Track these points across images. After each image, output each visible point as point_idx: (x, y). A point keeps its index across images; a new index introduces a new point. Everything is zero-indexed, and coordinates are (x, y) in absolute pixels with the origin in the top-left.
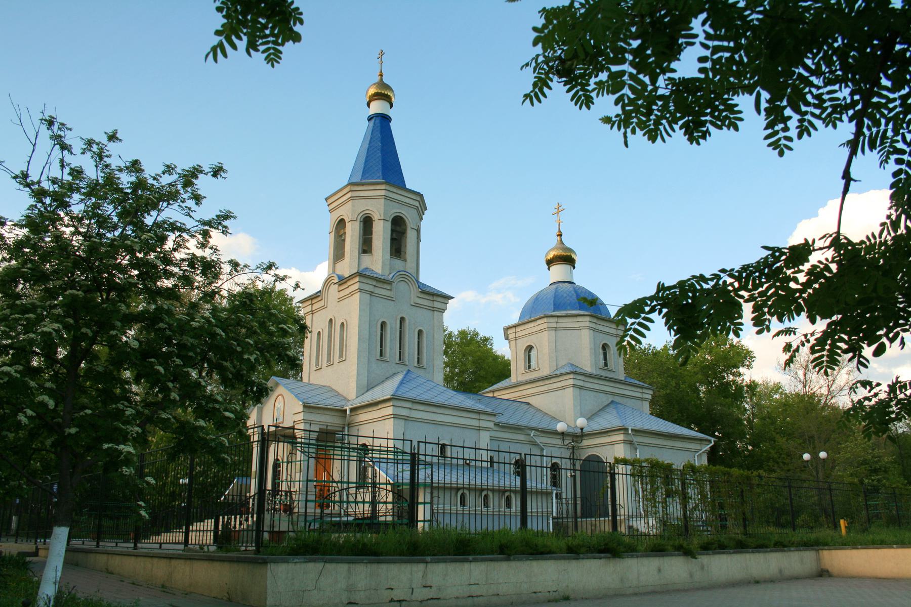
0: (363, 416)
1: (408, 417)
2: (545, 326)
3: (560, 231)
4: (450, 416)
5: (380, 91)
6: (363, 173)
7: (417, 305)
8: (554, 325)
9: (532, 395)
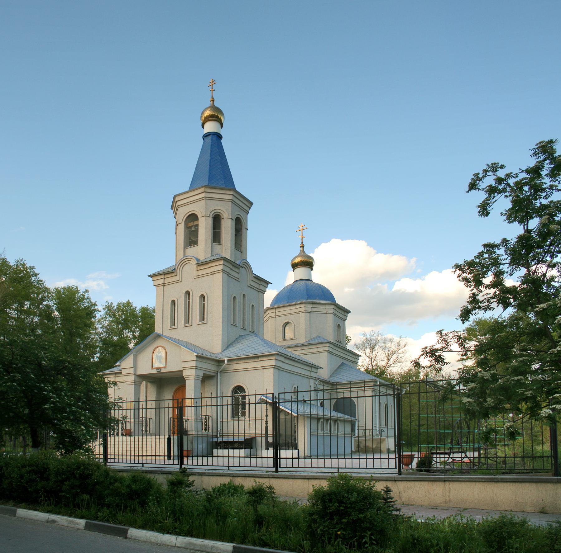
0: (238, 366)
1: (281, 367)
2: (303, 309)
3: (302, 243)
4: (299, 369)
5: (213, 113)
6: (209, 178)
7: (251, 287)
8: (309, 309)
9: (305, 354)
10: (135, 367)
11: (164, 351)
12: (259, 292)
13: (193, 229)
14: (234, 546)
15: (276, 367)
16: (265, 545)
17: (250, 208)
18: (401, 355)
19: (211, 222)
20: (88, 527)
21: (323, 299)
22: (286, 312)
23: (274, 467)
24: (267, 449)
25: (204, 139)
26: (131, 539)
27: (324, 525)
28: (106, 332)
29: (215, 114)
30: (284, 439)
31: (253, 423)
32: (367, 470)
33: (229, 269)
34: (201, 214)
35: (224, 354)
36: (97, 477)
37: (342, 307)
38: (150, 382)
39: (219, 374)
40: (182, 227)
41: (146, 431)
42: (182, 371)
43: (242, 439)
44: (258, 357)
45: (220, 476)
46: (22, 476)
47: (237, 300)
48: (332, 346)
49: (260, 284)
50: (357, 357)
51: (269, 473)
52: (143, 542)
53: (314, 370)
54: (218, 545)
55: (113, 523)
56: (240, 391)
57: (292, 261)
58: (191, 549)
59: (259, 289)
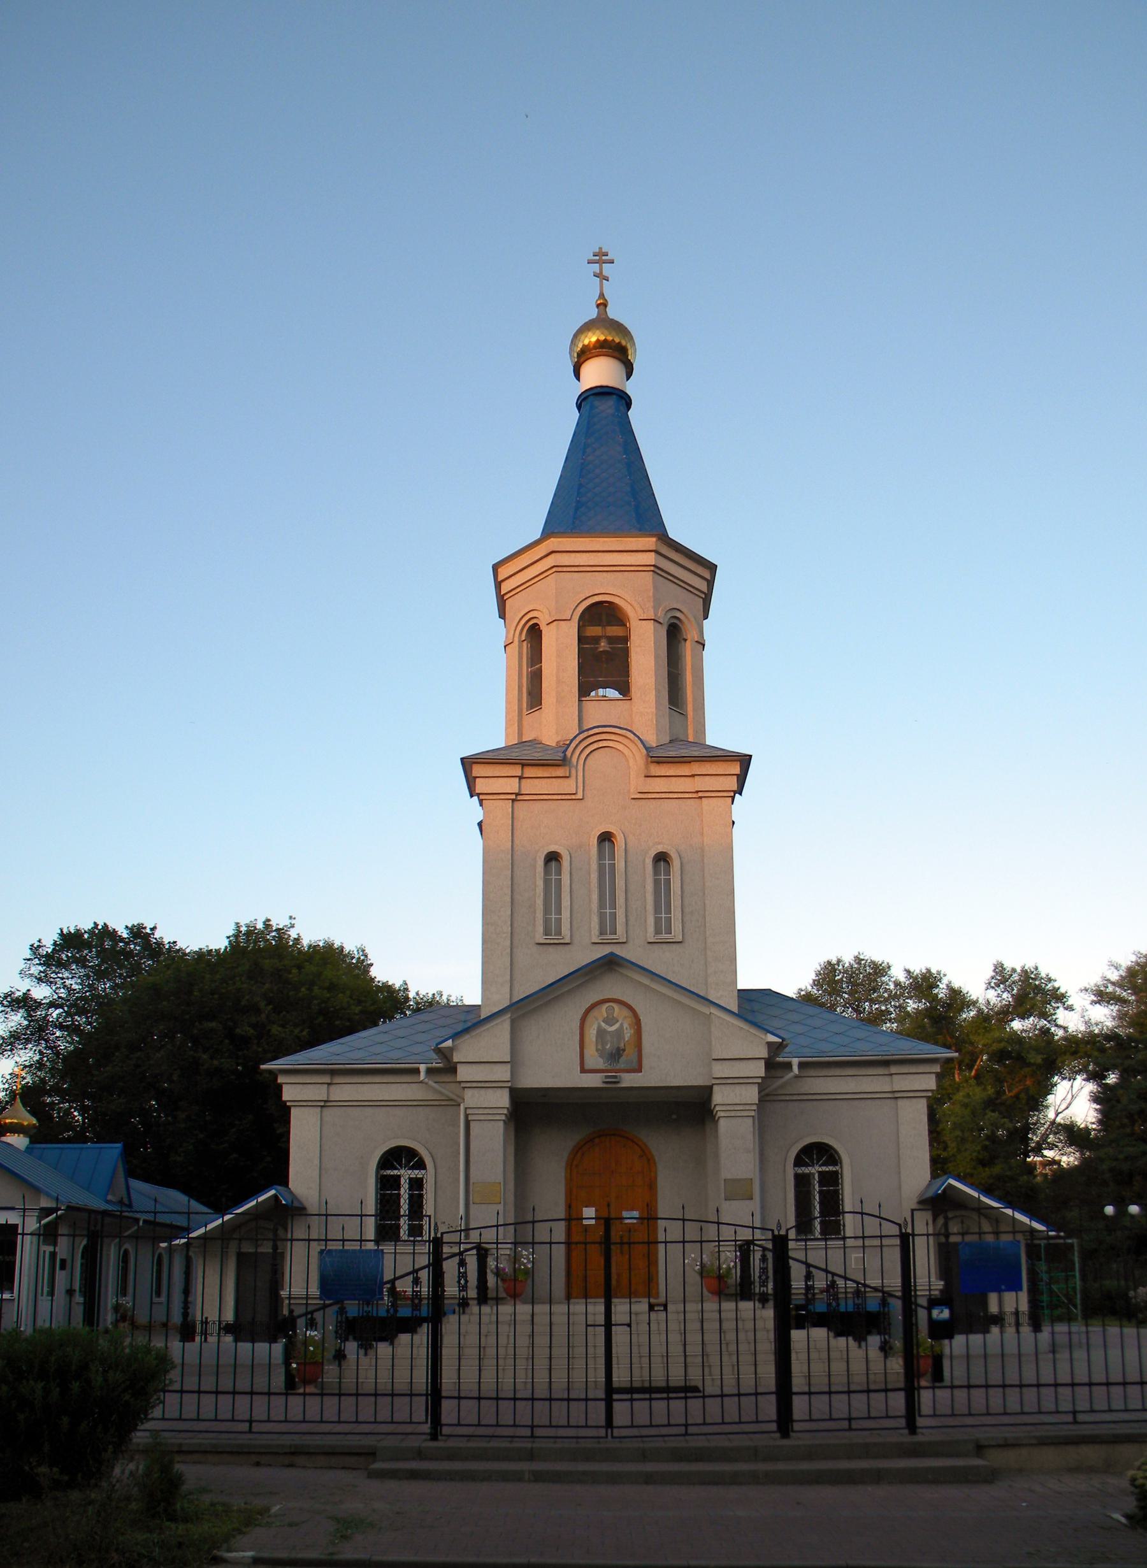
10: (514, 1062)
44: (886, 1063)
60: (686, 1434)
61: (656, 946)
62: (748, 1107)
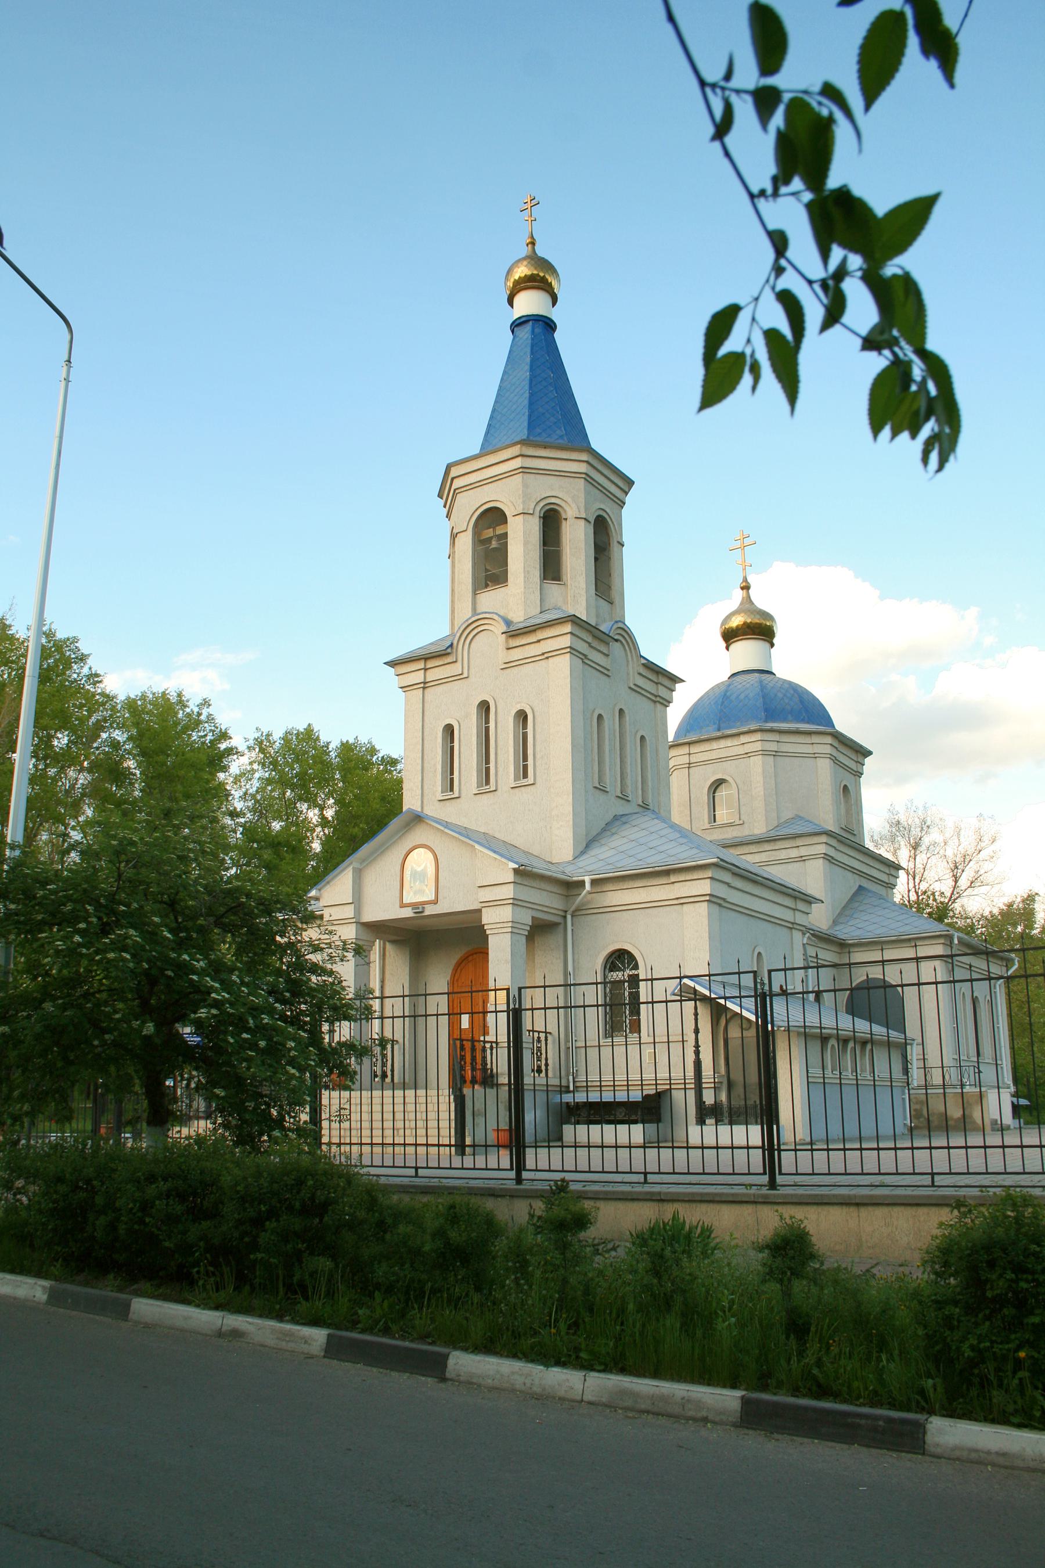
1: (724, 900)
2: (758, 746)
5: (535, 272)
7: (636, 690)
8: (773, 747)
9: (768, 863)
10: (357, 901)
11: (430, 856)
12: (655, 702)
13: (494, 544)
14: (743, 1397)
15: (713, 900)
16: (822, 1391)
17: (626, 493)
18: (987, 866)
19: (537, 528)
20: (333, 1349)
21: (803, 721)
22: (714, 755)
23: (764, 1173)
24: (701, 1121)
25: (513, 332)
26: (457, 1381)
27: (978, 1332)
28: (253, 810)
29: (538, 275)
30: (743, 1096)
31: (661, 1049)
32: (816, 1180)
33: (586, 645)
34: (512, 508)
35: (581, 864)
36: (351, 1207)
37: (852, 740)
38: (393, 942)
39: (569, 917)
40: (466, 542)
41: (384, 1075)
42: (479, 911)
43: (636, 1096)
44: (667, 873)
45: (626, 1200)
46: (146, 1206)
47: (607, 723)
48: (834, 842)
49: (657, 683)
50: (893, 872)
51: (753, 1190)
52: (492, 1389)
53: (801, 906)
54: (699, 1395)
55: (403, 1338)
56: (623, 963)
57: (723, 624)
58: (626, 1409)
59: (656, 696)
60: (646, 1182)
61: (517, 789)
62: (505, 925)
